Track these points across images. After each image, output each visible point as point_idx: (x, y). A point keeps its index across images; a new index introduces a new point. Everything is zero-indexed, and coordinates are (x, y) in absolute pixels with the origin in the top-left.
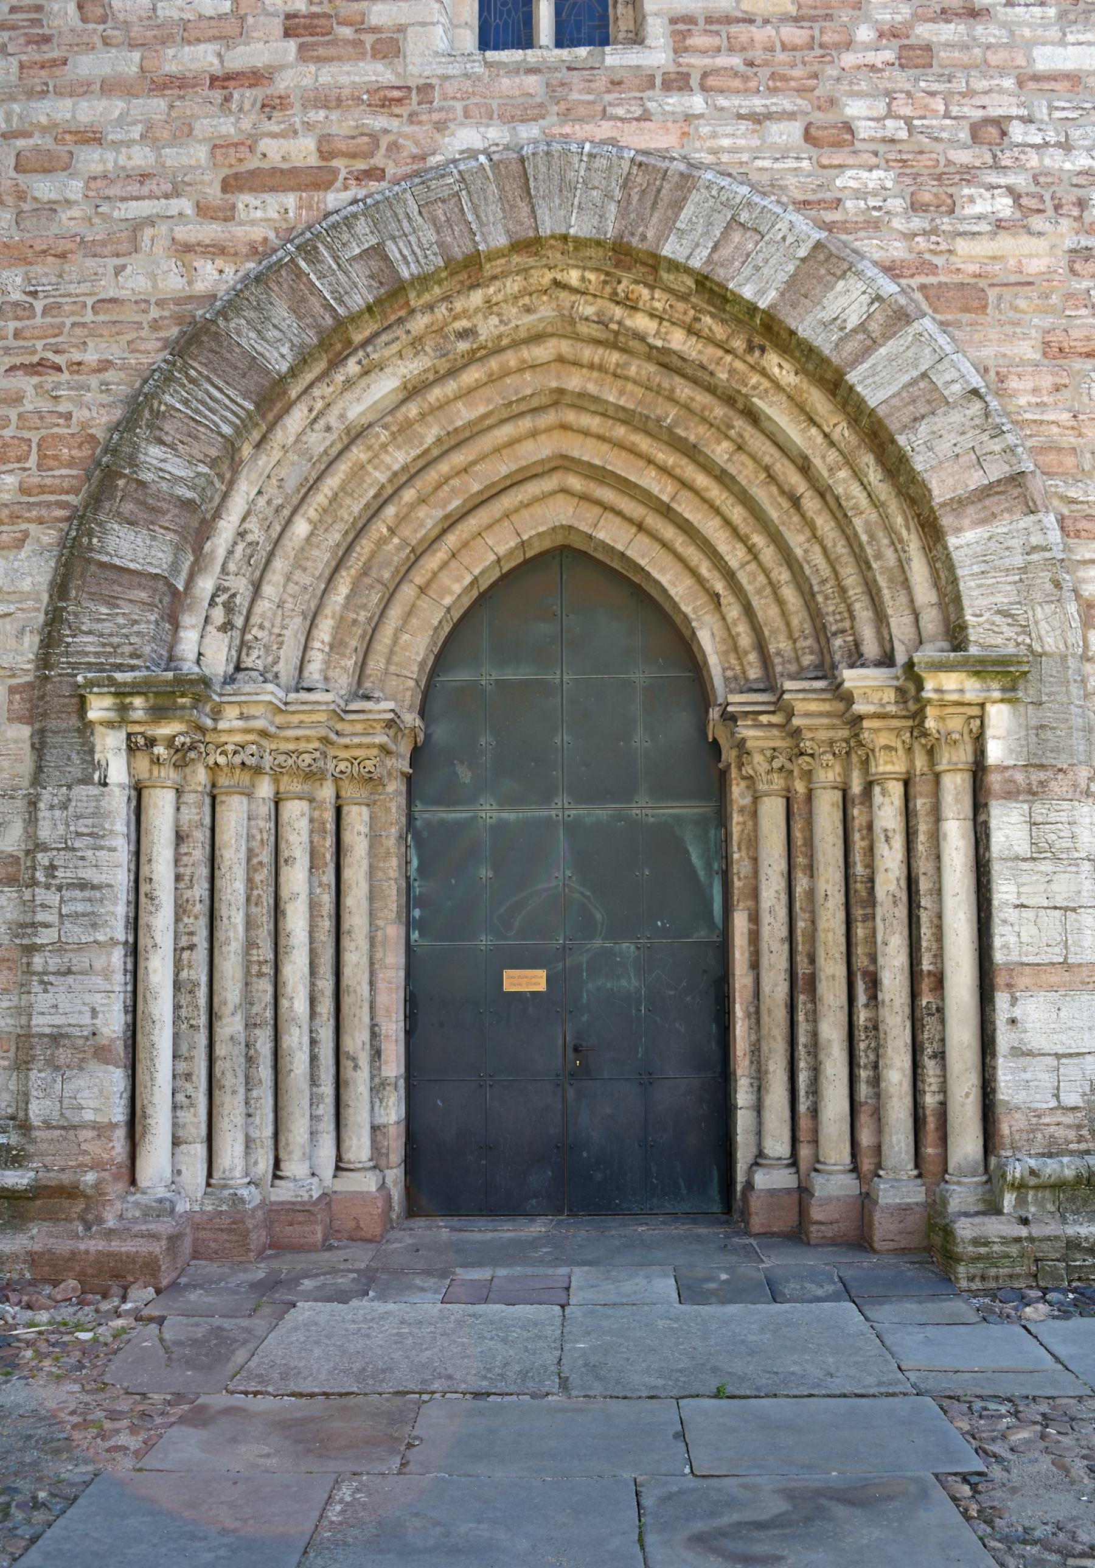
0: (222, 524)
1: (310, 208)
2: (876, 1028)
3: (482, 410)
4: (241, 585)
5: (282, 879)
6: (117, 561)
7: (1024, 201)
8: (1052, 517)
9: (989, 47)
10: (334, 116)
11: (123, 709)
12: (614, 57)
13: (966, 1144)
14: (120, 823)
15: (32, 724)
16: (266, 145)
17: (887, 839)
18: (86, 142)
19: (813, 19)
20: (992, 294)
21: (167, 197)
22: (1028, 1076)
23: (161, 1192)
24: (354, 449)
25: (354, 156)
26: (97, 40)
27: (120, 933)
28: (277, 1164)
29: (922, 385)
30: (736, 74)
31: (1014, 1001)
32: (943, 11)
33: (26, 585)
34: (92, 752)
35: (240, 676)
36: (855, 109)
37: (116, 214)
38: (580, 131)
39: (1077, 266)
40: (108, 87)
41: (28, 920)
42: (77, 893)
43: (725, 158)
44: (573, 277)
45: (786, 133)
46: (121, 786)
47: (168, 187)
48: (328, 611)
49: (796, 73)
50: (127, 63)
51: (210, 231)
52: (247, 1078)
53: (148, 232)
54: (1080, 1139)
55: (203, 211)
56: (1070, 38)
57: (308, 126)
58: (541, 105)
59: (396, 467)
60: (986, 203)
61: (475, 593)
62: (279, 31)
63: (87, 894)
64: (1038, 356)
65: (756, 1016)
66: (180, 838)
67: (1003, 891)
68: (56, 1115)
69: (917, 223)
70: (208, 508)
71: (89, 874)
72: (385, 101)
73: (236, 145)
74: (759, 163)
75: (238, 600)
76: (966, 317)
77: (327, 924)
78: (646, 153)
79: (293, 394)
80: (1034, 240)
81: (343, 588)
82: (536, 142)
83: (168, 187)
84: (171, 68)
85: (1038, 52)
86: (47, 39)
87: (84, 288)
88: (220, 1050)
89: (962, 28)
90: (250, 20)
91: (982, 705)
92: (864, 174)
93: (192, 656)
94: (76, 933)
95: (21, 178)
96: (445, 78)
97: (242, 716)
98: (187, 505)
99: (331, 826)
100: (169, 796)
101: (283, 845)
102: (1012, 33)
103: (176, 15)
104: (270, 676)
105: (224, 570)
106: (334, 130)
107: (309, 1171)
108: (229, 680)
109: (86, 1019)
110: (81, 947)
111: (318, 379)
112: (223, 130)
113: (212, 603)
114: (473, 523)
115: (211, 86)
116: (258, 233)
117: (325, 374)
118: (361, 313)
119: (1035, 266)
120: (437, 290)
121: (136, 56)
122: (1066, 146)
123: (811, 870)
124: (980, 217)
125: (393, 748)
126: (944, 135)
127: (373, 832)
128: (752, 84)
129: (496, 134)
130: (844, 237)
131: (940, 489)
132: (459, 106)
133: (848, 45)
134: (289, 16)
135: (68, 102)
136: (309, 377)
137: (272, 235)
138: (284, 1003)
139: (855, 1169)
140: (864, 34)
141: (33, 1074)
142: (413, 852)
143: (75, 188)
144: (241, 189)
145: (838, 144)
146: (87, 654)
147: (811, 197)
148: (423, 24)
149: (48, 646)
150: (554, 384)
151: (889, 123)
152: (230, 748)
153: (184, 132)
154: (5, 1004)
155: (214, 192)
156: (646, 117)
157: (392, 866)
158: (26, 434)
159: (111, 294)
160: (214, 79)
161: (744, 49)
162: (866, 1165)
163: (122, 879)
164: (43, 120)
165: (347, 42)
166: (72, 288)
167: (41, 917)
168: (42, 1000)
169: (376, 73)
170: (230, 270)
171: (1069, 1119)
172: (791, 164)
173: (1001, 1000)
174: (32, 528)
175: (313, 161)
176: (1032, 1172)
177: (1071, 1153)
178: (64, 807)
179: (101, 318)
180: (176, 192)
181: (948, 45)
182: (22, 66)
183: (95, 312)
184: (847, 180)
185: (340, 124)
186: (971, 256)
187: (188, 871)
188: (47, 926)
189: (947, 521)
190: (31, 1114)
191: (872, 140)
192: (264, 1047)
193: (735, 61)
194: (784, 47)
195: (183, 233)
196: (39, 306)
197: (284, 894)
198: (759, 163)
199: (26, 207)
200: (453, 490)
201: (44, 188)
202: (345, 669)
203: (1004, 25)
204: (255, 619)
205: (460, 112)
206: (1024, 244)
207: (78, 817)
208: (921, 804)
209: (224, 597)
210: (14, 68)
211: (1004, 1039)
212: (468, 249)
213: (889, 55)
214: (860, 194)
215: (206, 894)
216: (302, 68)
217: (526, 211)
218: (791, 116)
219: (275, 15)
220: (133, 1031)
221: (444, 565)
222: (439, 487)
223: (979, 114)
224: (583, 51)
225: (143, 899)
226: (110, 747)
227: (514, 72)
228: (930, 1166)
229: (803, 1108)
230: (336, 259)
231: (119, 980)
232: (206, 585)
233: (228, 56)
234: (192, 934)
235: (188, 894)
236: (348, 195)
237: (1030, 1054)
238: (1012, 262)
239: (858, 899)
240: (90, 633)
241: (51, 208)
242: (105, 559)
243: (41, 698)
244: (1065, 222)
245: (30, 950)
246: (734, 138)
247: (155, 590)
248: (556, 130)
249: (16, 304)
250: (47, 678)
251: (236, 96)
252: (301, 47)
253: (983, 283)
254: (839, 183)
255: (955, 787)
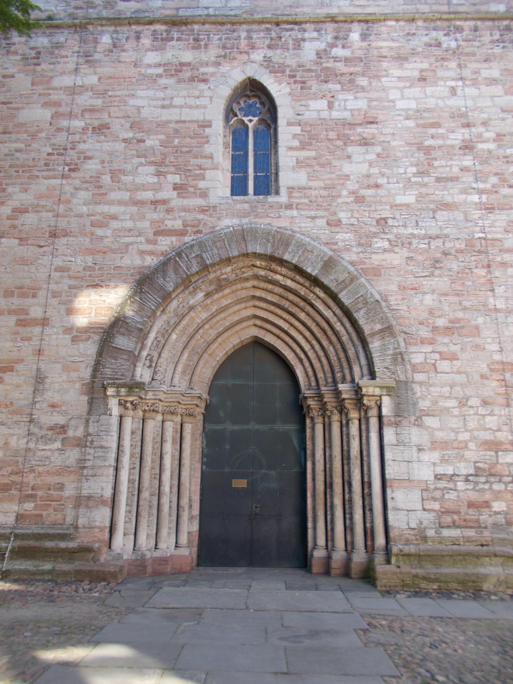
0: (150, 335)
1: (180, 241)
2: (351, 500)
3: (230, 301)
4: (156, 355)
5: (163, 447)
6: (118, 346)
7: (392, 243)
8: (402, 339)
9: (382, 196)
10: (187, 214)
11: (118, 392)
12: (271, 199)
13: (380, 540)
14: (115, 428)
15: (88, 395)
16: (167, 222)
17: (354, 438)
18: (113, 219)
19: (329, 188)
20: (383, 271)
21: (137, 236)
22: (398, 517)
23: (119, 551)
24: (191, 313)
25: (193, 226)
26: (116, 188)
27: (113, 463)
28: (156, 545)
29: (361, 298)
30: (306, 205)
31: (393, 491)
32: (368, 186)
33: (89, 352)
34: (107, 405)
35: (153, 382)
36: (342, 215)
37: (121, 241)
38: (260, 221)
39: (408, 262)
40: (120, 203)
41: (83, 458)
42: (100, 450)
43: (303, 229)
44: (258, 263)
45: (321, 222)
46: (116, 416)
47: (137, 234)
48: (181, 362)
49: (324, 204)
50: (126, 196)
51: (150, 247)
52: (149, 513)
53: (131, 247)
54: (417, 539)
55: (148, 241)
56: (407, 193)
57: (180, 217)
58: (249, 213)
59: (203, 318)
60: (380, 244)
61: (226, 356)
62: (172, 188)
63: (103, 450)
64: (397, 289)
65: (314, 496)
66: (133, 433)
67: (388, 455)
68: (87, 524)
69: (360, 249)
70: (146, 331)
71: (104, 444)
72: (203, 210)
73: (158, 222)
74: (313, 231)
75: (154, 358)
76: (375, 278)
77: (177, 462)
78: (280, 228)
79: (173, 297)
80: (395, 255)
81: (186, 355)
82: (247, 224)
83: (137, 234)
84: (139, 198)
85: (397, 198)
86: (101, 187)
87: (111, 263)
88: (141, 503)
89: (374, 191)
90: (163, 185)
91: (380, 397)
92: (344, 235)
93: (139, 376)
94: (98, 463)
95: (93, 229)
96: (220, 204)
97: (153, 395)
98: (141, 330)
99: (179, 430)
100: (130, 419)
101: (164, 436)
102: (389, 192)
103: (141, 182)
104: (162, 382)
105: (150, 349)
106: (187, 218)
107: (167, 544)
108: (150, 383)
109: (99, 491)
110: (100, 467)
111: (181, 292)
112: (154, 217)
113: (146, 359)
114: (226, 334)
115: (151, 204)
116: (164, 248)
117: (183, 290)
118: (194, 274)
119: (396, 262)
120: (217, 267)
121: (128, 194)
122: (405, 226)
123: (331, 447)
124: (379, 248)
125: (199, 405)
126: (368, 223)
127: (193, 431)
128: (311, 208)
129: (236, 221)
130: (339, 253)
131: (367, 330)
132: (224, 212)
133: (340, 196)
134: (175, 184)
135: (107, 206)
136: (178, 291)
137: (168, 249)
138: (162, 488)
139: (346, 550)
140: (344, 193)
141: (81, 510)
142: (204, 439)
143: (109, 233)
144: (159, 235)
145: (337, 226)
146: (107, 374)
147: (328, 242)
148: (214, 188)
149: (95, 371)
150: (252, 294)
151: (352, 219)
152: (150, 404)
153: (143, 217)
154: (73, 486)
155: (151, 236)
156: (280, 217)
157: (198, 443)
158: (91, 306)
159: (119, 265)
160: (152, 202)
161: (309, 197)
162: (349, 548)
163: (114, 445)
164: (100, 211)
165: (192, 192)
166: (107, 263)
167: (88, 457)
168: (86, 485)
169: (200, 202)
170: (155, 259)
171: (412, 532)
172: (323, 232)
173: (389, 491)
174: (92, 335)
175: (181, 227)
176: (401, 551)
177: (414, 544)
178: (98, 422)
179: (116, 272)
180: (140, 235)
181: (370, 196)
182: (93, 195)
183: (114, 270)
184: (339, 236)
185: (189, 217)
186: (376, 259)
187: (134, 443)
188: (89, 460)
189: (369, 340)
190: (79, 523)
191: (347, 224)
192: (155, 503)
193: (306, 201)
194: (321, 197)
195: (142, 247)
196: (97, 267)
197: (164, 452)
198: (313, 231)
199: (94, 237)
200: (220, 324)
201: (99, 232)
202: (185, 380)
203: (386, 190)
204: (158, 364)
205: (225, 214)
206: (392, 256)
207: (102, 425)
208: (363, 427)
209: (150, 357)
210: (91, 195)
211: (390, 504)
212: (227, 256)
213: (352, 199)
214: (343, 241)
215: (139, 451)
216: (178, 200)
217: (244, 245)
218: (323, 217)
219: (170, 183)
220: (114, 495)
221: (217, 347)
222: (216, 323)
223: (379, 217)
224: (261, 197)
225: (120, 452)
226: (113, 404)
227: (241, 203)
228: (370, 548)
229: (329, 528)
230: (188, 257)
231: (111, 479)
232: (145, 353)
233: (156, 195)
234: (134, 464)
235: (134, 451)
236: (191, 238)
237: (398, 509)
238: (389, 261)
239: (346, 457)
240: (108, 368)
241: (102, 238)
242: (115, 345)
243: (93, 387)
244: (405, 249)
245: (84, 468)
246: (306, 225)
247: (130, 356)
248: (253, 220)
249: (90, 267)
250: (94, 381)
251: (158, 207)
252: (178, 194)
253: (380, 268)
254: (337, 237)
255: (374, 422)
